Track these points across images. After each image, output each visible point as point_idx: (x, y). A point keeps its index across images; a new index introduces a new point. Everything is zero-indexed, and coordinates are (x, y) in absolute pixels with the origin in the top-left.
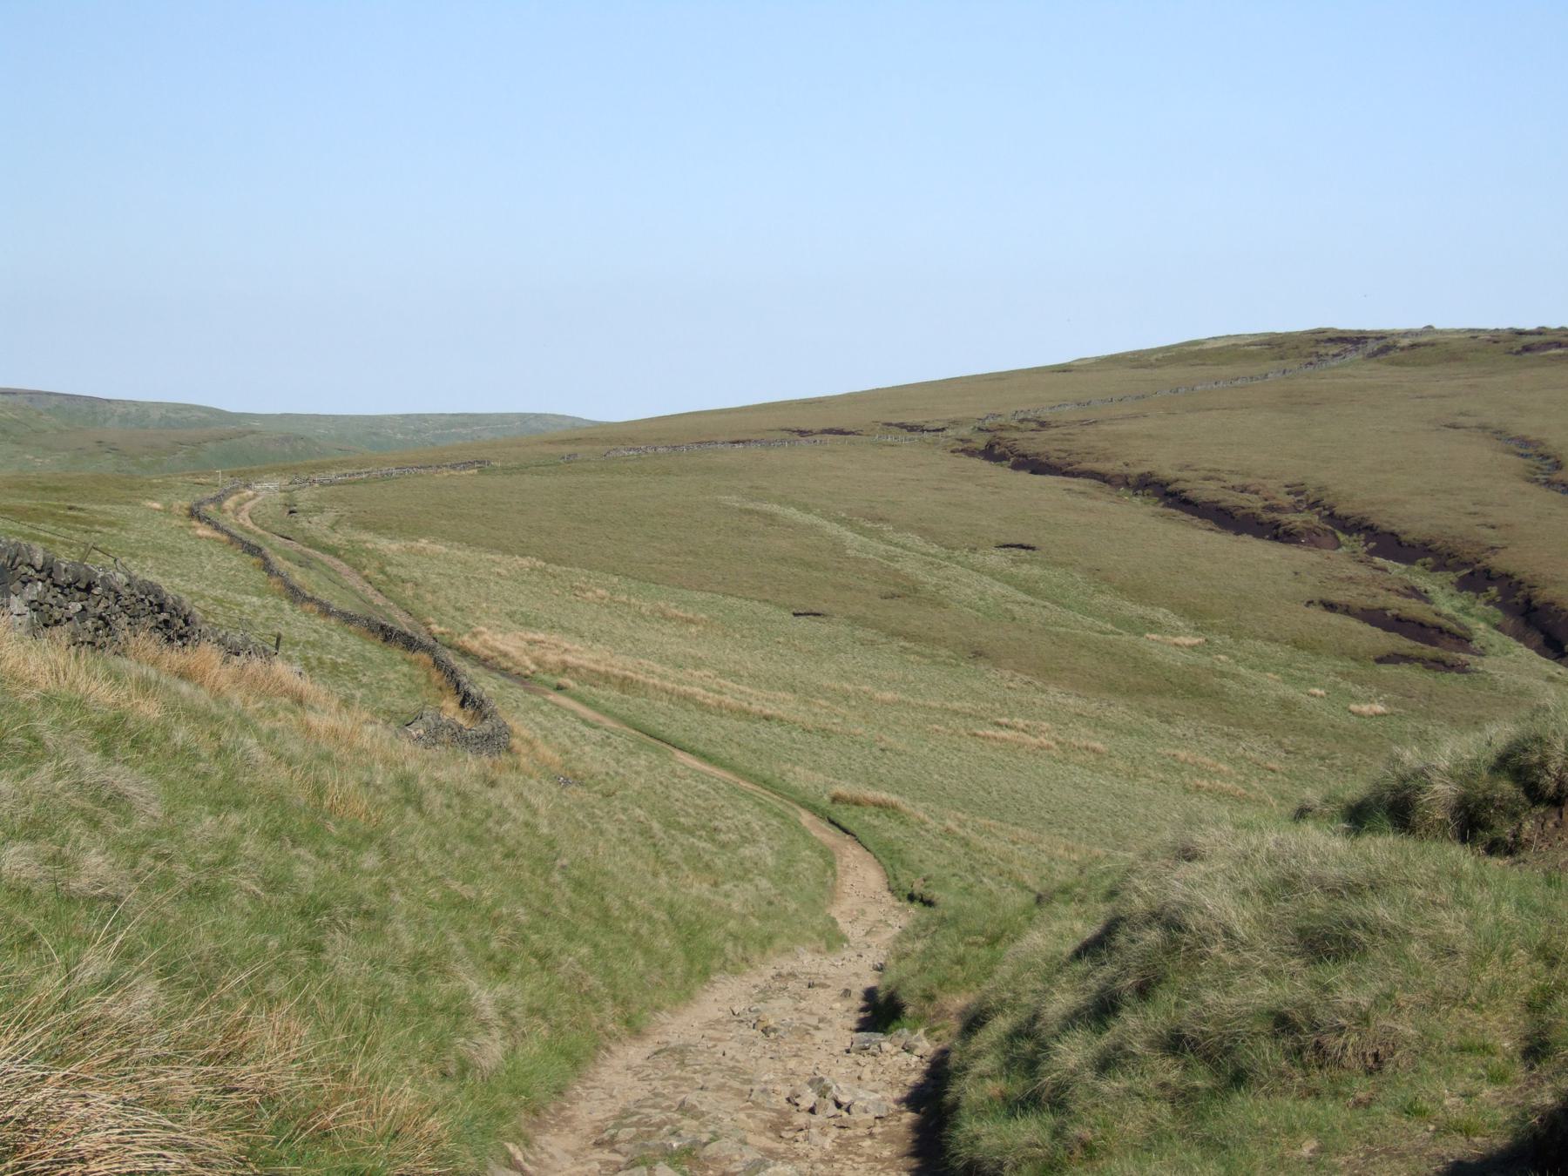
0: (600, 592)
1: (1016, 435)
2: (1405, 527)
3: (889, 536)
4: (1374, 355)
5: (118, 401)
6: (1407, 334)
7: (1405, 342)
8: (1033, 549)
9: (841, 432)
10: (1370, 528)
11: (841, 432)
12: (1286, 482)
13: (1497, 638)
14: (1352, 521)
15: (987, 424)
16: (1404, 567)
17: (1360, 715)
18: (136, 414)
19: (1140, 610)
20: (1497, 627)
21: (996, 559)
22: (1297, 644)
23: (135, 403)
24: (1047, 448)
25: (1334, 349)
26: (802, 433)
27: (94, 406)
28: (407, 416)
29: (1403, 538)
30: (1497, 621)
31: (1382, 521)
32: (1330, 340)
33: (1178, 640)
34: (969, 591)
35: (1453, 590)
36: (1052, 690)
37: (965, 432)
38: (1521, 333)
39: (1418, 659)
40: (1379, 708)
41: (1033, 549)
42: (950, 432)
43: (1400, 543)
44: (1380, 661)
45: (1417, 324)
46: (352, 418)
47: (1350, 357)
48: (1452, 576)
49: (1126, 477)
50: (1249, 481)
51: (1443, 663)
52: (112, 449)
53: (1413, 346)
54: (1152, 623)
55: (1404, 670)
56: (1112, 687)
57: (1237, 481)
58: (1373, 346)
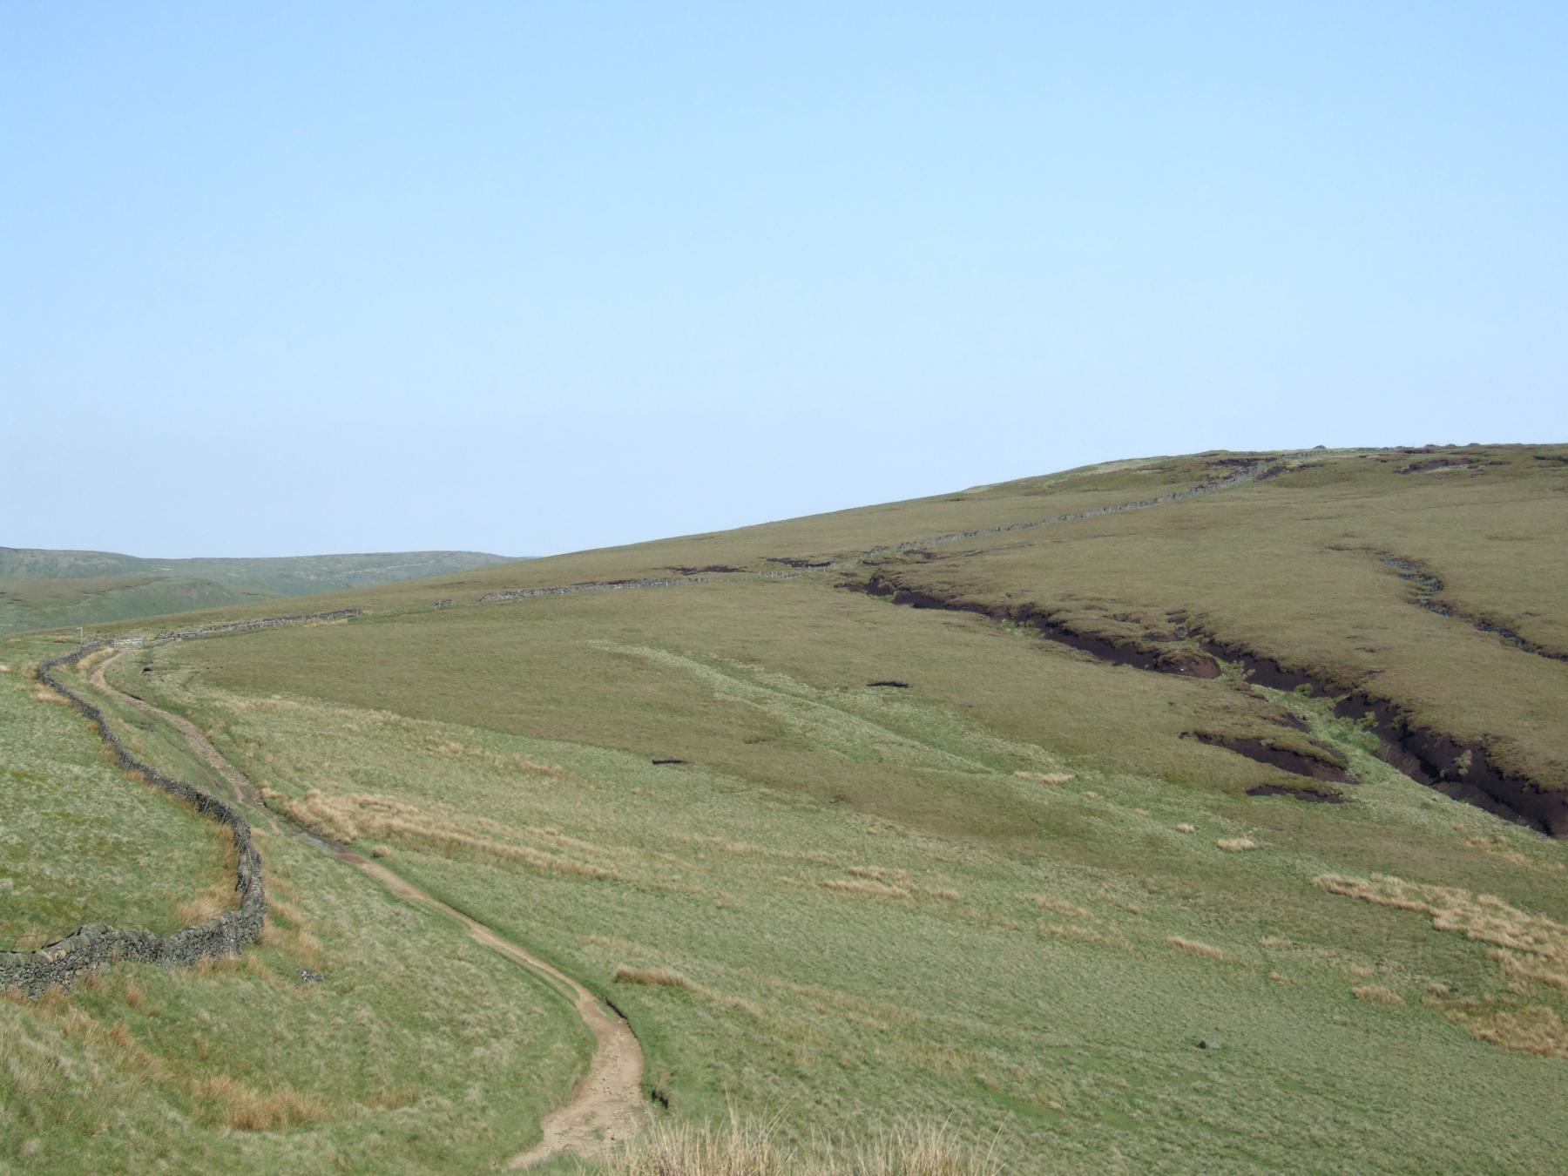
1: (901, 569)
2: (1284, 653)
3: (759, 677)
4: (1264, 476)
6: (1295, 455)
7: (1295, 463)
8: (906, 686)
9: (725, 569)
10: (1250, 655)
11: (725, 569)
12: (1168, 609)
13: (1374, 764)
14: (1232, 648)
15: (872, 558)
16: (1283, 693)
17: (1227, 850)
19: (1011, 747)
20: (1375, 753)
21: (868, 698)
22: (1169, 778)
23: (43, 552)
25: (1225, 472)
26: (685, 571)
28: (319, 558)
29: (1282, 664)
30: (1375, 747)
31: (1263, 646)
32: (1222, 463)
35: (1330, 716)
36: (913, 833)
37: (849, 566)
38: (1410, 451)
40: (1248, 843)
41: (906, 686)
42: (835, 567)
44: (1252, 792)
45: (1308, 445)
47: (1240, 479)
48: (1330, 702)
49: (1008, 608)
50: (1128, 610)
51: (1316, 793)
53: (1303, 467)
55: (1277, 802)
57: (1119, 609)
58: (1263, 468)
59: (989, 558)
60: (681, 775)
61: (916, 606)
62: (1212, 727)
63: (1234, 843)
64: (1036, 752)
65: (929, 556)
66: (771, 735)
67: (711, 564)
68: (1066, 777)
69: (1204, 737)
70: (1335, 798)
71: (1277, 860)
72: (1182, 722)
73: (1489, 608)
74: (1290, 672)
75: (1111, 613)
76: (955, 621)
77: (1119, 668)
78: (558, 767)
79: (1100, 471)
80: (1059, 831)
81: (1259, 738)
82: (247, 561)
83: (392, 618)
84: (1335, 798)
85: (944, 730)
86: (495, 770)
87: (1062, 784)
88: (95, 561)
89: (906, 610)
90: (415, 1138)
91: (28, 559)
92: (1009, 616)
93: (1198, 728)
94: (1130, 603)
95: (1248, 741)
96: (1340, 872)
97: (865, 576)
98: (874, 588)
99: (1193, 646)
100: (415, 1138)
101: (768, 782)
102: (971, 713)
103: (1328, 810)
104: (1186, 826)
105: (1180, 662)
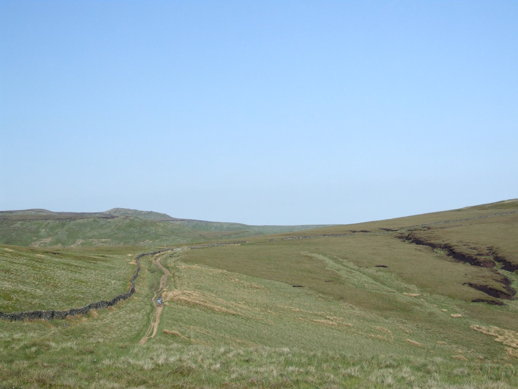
0: (236, 280)
1: (415, 234)
3: (344, 263)
5: (214, 222)
8: (386, 267)
9: (366, 231)
10: (505, 261)
11: (366, 231)
15: (411, 229)
17: (452, 317)
18: (220, 226)
19: (406, 285)
21: (372, 270)
22: (450, 296)
23: (219, 223)
24: (424, 236)
26: (354, 232)
27: (207, 224)
28: (303, 226)
29: (512, 264)
31: (508, 259)
33: (411, 294)
34: (355, 280)
36: (357, 309)
37: (403, 231)
39: (486, 301)
40: (460, 315)
41: (386, 267)
42: (398, 231)
43: (511, 265)
44: (474, 301)
46: (285, 226)
49: (441, 245)
52: (204, 237)
54: (408, 289)
55: (480, 305)
56: (377, 308)
57: (473, 246)
59: (446, 229)
60: (298, 290)
61: (417, 244)
62: (474, 282)
63: (455, 315)
64: (413, 287)
65: (429, 228)
66: (335, 279)
67: (362, 230)
68: (417, 295)
69: (471, 285)
70: (502, 304)
71: (465, 321)
72: (466, 280)
73: (447, 242)
74: (514, 266)
75: (470, 247)
76: (418, 248)
77: (458, 264)
78: (263, 287)
79: (505, 202)
80: (405, 311)
81: (487, 286)
82: (280, 227)
83: (253, 244)
84: (502, 304)
85: (389, 280)
86: (244, 287)
87: (415, 297)
88: (234, 226)
89: (414, 245)
90: (40, 316)
91: (215, 225)
92: (440, 247)
93: (470, 282)
94: (478, 244)
95: (484, 286)
96: (479, 324)
97: (406, 234)
98: (408, 238)
99: (491, 258)
100: (40, 316)
101: (323, 293)
102: (401, 276)
103: (496, 308)
104: (445, 310)
105: (481, 262)
